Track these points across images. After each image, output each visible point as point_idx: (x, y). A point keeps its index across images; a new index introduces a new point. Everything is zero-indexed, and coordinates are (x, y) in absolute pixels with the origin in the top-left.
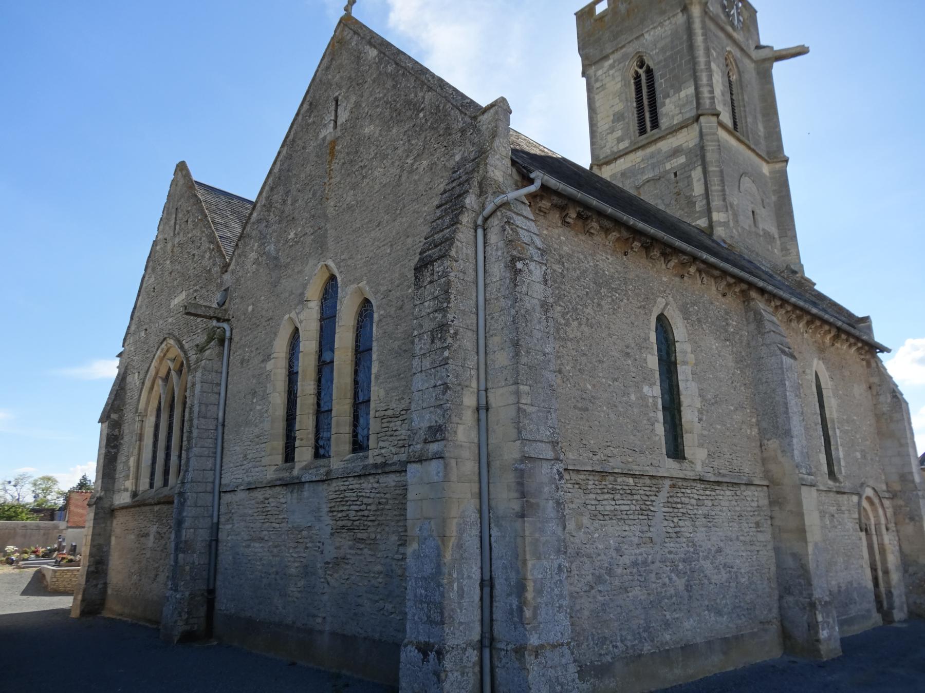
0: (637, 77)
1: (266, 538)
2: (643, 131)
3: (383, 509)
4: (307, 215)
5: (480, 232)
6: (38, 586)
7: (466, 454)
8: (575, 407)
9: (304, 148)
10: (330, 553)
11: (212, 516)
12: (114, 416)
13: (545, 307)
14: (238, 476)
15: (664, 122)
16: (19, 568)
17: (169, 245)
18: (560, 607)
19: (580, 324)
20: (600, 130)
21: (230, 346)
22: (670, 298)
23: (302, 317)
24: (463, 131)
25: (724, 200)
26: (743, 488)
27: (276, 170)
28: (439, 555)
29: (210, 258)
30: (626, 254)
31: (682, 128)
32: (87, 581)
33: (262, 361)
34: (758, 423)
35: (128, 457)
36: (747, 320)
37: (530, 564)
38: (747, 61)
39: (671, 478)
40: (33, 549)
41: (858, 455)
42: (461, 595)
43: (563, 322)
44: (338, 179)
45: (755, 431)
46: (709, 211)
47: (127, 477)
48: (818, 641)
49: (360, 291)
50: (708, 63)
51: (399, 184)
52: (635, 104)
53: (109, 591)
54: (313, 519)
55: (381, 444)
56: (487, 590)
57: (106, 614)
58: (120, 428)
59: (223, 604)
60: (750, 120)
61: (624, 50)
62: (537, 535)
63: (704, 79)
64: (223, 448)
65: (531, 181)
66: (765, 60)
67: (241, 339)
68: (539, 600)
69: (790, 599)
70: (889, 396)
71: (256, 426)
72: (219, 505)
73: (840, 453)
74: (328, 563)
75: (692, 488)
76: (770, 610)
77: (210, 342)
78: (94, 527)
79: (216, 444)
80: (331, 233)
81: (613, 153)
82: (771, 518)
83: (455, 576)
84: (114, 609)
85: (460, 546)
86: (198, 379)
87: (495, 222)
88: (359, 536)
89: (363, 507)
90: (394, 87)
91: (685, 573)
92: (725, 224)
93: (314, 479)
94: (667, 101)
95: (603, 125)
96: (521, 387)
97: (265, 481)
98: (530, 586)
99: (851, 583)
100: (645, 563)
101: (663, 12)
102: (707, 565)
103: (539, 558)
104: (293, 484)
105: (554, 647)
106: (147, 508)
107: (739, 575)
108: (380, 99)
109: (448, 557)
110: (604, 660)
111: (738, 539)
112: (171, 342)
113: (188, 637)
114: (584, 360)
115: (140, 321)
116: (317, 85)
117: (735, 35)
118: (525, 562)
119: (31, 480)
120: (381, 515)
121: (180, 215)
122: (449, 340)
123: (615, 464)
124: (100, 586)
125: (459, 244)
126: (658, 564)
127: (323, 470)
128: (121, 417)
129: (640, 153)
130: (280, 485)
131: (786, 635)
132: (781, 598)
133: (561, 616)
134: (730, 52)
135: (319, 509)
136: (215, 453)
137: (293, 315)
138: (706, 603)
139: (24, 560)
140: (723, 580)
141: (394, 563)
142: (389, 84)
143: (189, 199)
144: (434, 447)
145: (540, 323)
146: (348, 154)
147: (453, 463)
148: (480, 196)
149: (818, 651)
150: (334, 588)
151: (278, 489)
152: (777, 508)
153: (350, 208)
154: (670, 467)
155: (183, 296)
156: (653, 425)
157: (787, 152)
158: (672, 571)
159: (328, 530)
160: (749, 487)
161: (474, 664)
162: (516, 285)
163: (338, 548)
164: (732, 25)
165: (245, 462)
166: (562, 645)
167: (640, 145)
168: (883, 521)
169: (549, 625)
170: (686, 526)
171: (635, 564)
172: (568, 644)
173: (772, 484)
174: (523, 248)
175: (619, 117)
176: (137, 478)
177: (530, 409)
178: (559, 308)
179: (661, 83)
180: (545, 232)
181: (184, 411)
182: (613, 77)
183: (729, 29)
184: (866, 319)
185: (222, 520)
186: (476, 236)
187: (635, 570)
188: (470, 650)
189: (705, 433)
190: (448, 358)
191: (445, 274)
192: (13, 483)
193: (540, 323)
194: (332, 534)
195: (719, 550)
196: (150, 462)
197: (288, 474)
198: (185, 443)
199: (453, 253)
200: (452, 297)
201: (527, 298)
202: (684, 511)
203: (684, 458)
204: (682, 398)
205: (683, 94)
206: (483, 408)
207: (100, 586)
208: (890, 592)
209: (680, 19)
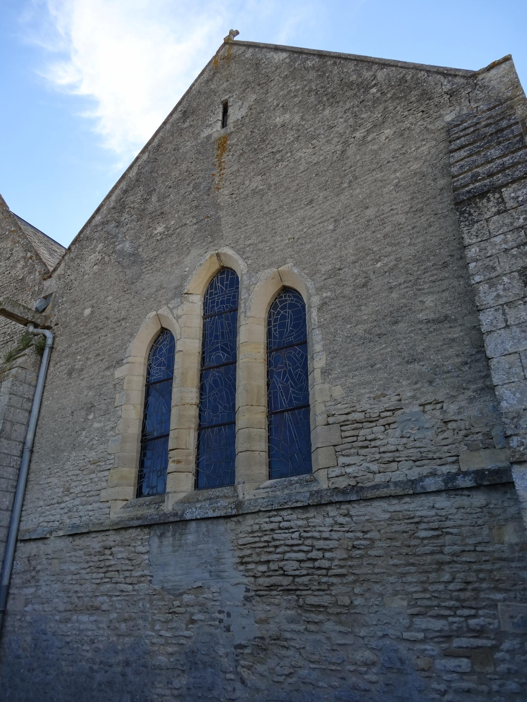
1: (104, 607)
3: (361, 557)
10: (245, 627)
14: (52, 518)
21: (50, 357)
33: (108, 368)
54: (207, 575)
55: (342, 460)
64: (27, 481)
67: (70, 346)
71: (91, 449)
72: (14, 559)
74: (241, 646)
77: (24, 349)
79: (19, 475)
89: (314, 554)
93: (211, 514)
97: (107, 522)
120: (360, 566)
130: (137, 527)
135: (218, 560)
136: (16, 487)
137: (163, 311)
141: (402, 647)
144: (249, 594)
150: (258, 690)
151: (133, 533)
159: (240, 593)
163: (265, 621)
165: (67, 499)
185: (17, 580)
186: (10, 578)
194: (247, 599)
197: (152, 511)
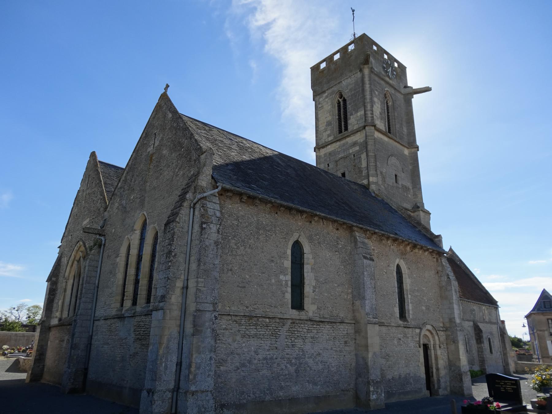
0: (339, 103)
2: (340, 132)
4: (139, 189)
5: (192, 209)
6: (15, 367)
7: (175, 307)
8: (238, 286)
9: (141, 155)
11: (89, 332)
12: (54, 279)
13: (217, 243)
15: (350, 128)
16: (7, 357)
17: (85, 194)
18: (209, 375)
19: (245, 248)
20: (320, 130)
22: (302, 233)
23: (132, 238)
24: (195, 161)
25: (376, 171)
26: (338, 324)
27: (130, 164)
28: (158, 351)
29: (100, 203)
30: (277, 213)
31: (358, 132)
32: (34, 364)
34: (352, 293)
35: (59, 300)
36: (351, 241)
37: (194, 356)
38: (398, 95)
39: (292, 319)
40: (18, 347)
41: (424, 308)
42: (166, 368)
43: (235, 247)
44: (152, 173)
45: (350, 296)
46: (368, 177)
47: (57, 311)
48: (370, 400)
49: (155, 228)
50: (371, 99)
51: (172, 181)
52: (337, 117)
53: (45, 370)
56: (179, 367)
57: (43, 381)
58: (56, 285)
59: (91, 376)
60: (398, 126)
61: (333, 89)
62: (200, 344)
63: (369, 107)
64: (97, 299)
65: (217, 187)
66: (408, 94)
68: (197, 371)
69: (360, 379)
70: (446, 277)
73: (410, 307)
74: (131, 355)
75: (304, 324)
76: (349, 385)
78: (40, 336)
79: (94, 296)
80: (147, 199)
81: (326, 142)
82: (355, 339)
83: (164, 360)
84: (47, 378)
85: (167, 347)
86: (87, 264)
87: (198, 206)
88: (143, 343)
90: (175, 133)
91: (296, 364)
92: (376, 183)
94: (352, 117)
95: (322, 127)
96: (199, 279)
98: (193, 366)
99: (409, 374)
100: (271, 358)
101: (351, 71)
102: (310, 362)
103: (200, 353)
104: (121, 318)
105: (203, 392)
106: (65, 327)
107: (331, 367)
108: (170, 138)
109: (161, 352)
110: (241, 402)
111: (332, 349)
112: (81, 243)
113: (73, 391)
114: (246, 264)
115: (69, 230)
116: (150, 126)
117: (391, 82)
118: (192, 356)
119: (27, 307)
121: (90, 179)
122: (172, 258)
123: (259, 312)
124: (40, 367)
125: (181, 215)
126: (279, 359)
127: (133, 312)
128: (57, 279)
129: (338, 143)
131: (357, 397)
132: (357, 379)
133: (209, 379)
134: (387, 91)
138: (308, 379)
139: (11, 353)
140: (320, 368)
142: (174, 132)
143: (96, 169)
144: (161, 304)
145: (213, 251)
146: (157, 162)
147: (168, 311)
148: (194, 193)
149: (369, 405)
151: (116, 320)
152: (357, 335)
153: (154, 188)
154: (294, 313)
155: (88, 220)
156: (284, 294)
157: (418, 143)
158: (287, 363)
160: (341, 324)
161: (169, 398)
162: (201, 235)
163: (135, 348)
164: (388, 76)
166: (208, 391)
167: (338, 139)
168: (437, 342)
169: (205, 382)
170: (299, 343)
171: (265, 359)
172: (211, 391)
173: (356, 322)
174: (208, 218)
175: (329, 124)
176: (62, 312)
177: (202, 289)
178: (234, 241)
179: (349, 107)
180: (230, 206)
181: (79, 280)
182: (327, 103)
183: (387, 79)
184: (439, 236)
185: (94, 334)
187: (265, 362)
188: (168, 392)
189: (316, 297)
190: (170, 266)
191: (173, 229)
192: (16, 309)
193: (213, 251)
195: (319, 354)
196: (68, 304)
198: (79, 296)
199: (177, 220)
200: (175, 239)
201: (207, 240)
202: (299, 335)
203: (304, 309)
204: (305, 281)
205: (359, 114)
206: (186, 288)
207: (40, 367)
208: (439, 380)
209: (359, 75)
